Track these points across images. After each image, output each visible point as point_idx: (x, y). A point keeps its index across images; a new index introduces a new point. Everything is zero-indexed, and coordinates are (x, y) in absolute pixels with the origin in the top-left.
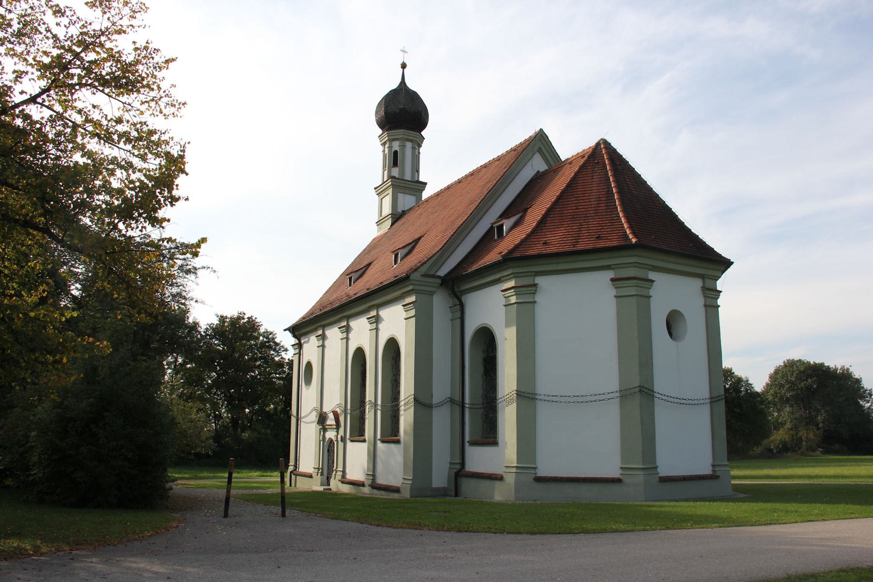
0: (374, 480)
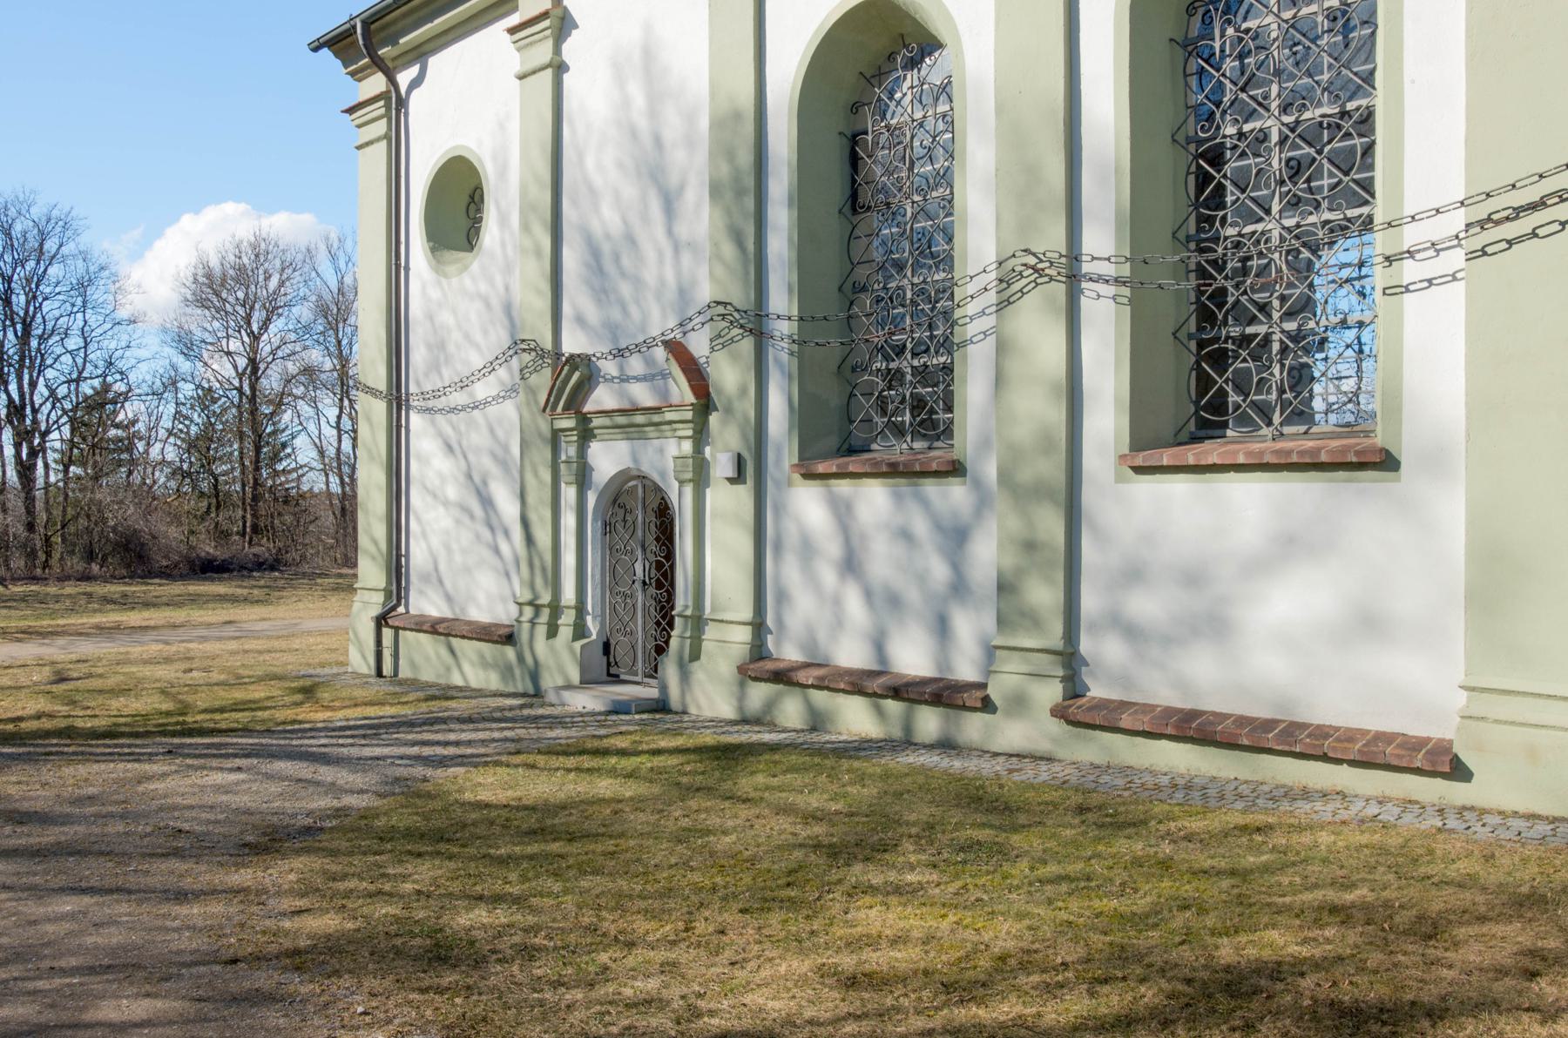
0: (1074, 689)
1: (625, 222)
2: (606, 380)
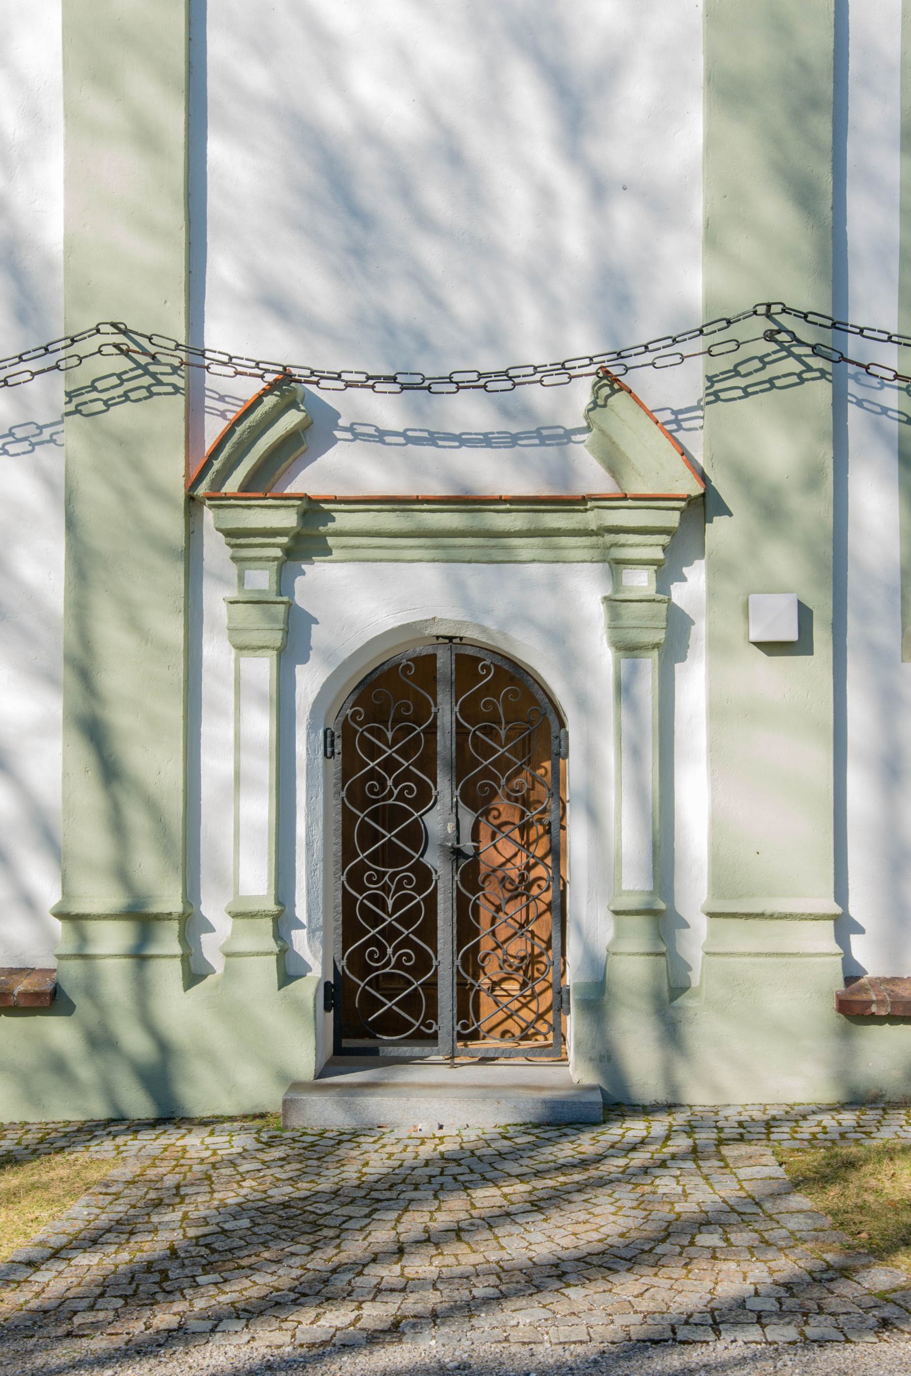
1: (433, 115)
2: (356, 436)
